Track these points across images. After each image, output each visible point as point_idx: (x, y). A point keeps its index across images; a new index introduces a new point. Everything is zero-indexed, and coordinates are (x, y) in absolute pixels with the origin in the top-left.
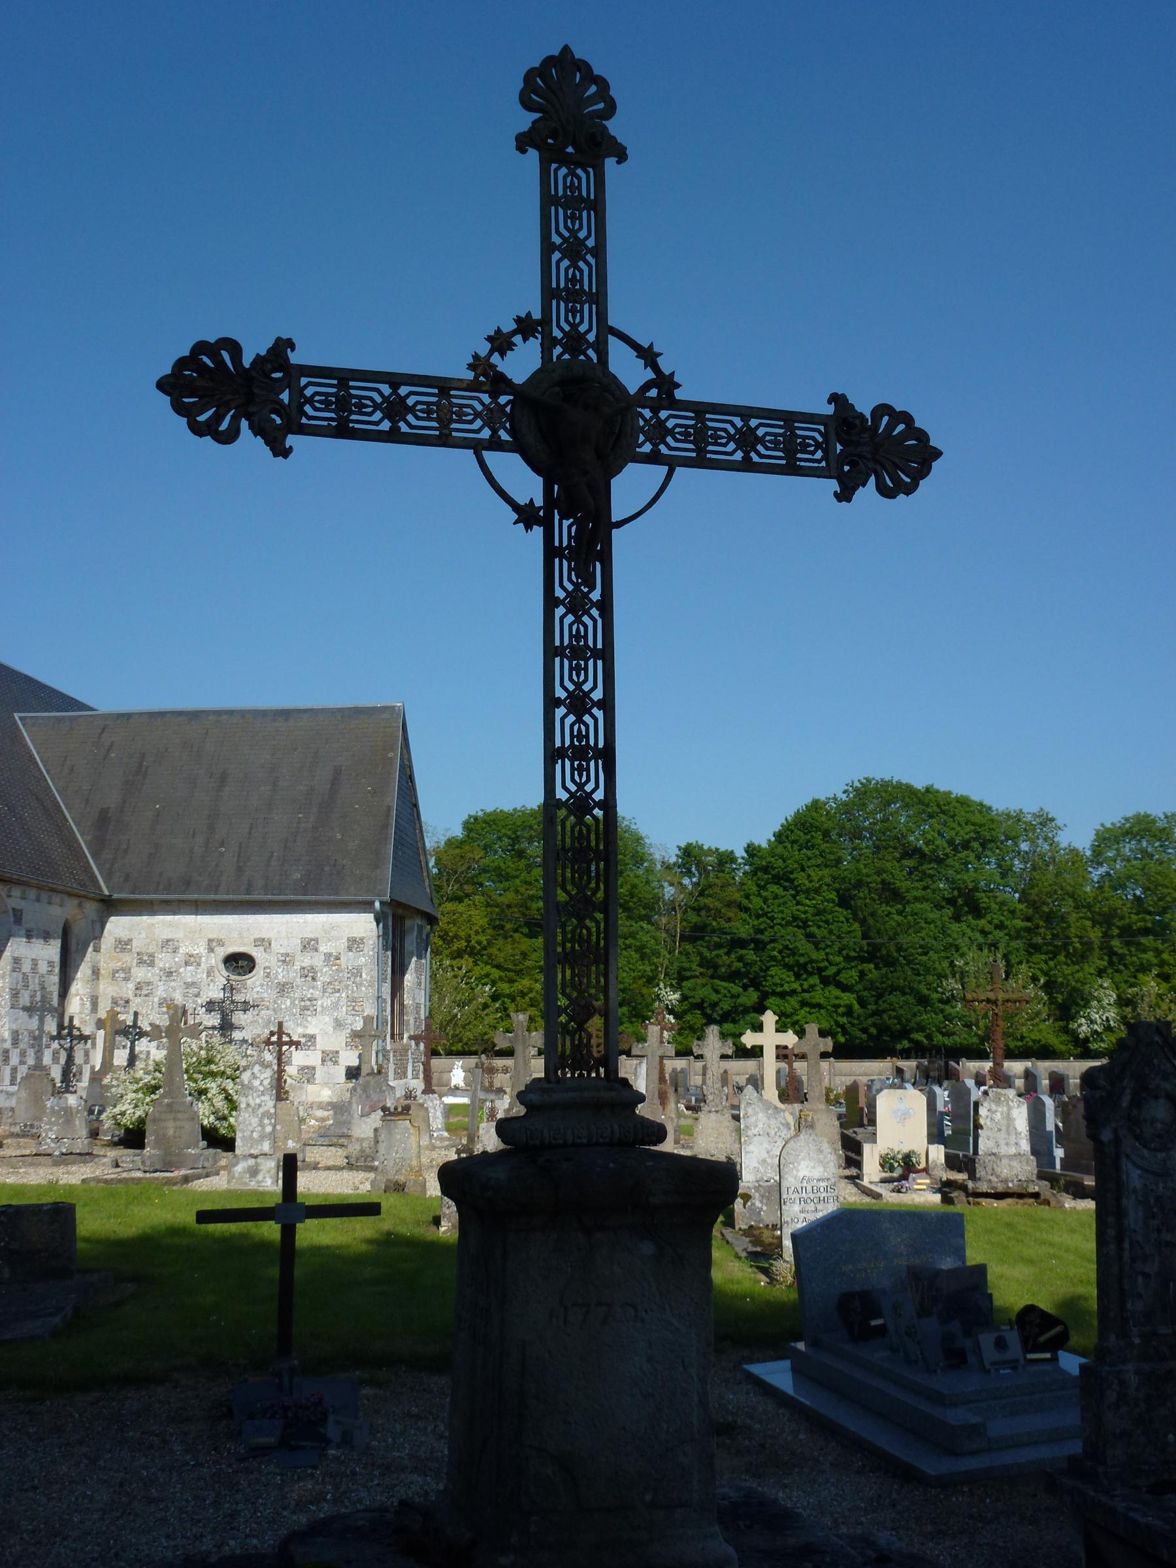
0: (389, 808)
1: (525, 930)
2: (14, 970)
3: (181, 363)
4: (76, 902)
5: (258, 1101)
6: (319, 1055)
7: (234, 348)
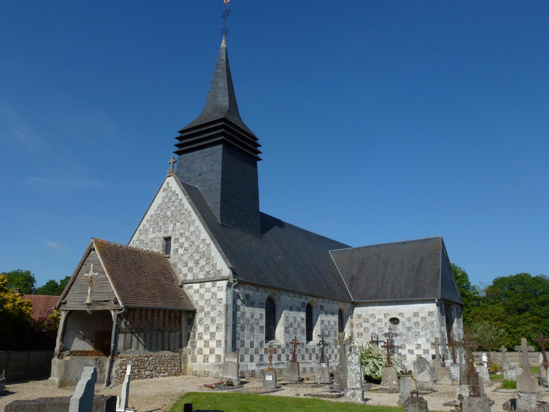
0: (439, 269)
1: (517, 312)
2: (321, 324)
4: (343, 303)
5: (354, 368)
6: (423, 351)
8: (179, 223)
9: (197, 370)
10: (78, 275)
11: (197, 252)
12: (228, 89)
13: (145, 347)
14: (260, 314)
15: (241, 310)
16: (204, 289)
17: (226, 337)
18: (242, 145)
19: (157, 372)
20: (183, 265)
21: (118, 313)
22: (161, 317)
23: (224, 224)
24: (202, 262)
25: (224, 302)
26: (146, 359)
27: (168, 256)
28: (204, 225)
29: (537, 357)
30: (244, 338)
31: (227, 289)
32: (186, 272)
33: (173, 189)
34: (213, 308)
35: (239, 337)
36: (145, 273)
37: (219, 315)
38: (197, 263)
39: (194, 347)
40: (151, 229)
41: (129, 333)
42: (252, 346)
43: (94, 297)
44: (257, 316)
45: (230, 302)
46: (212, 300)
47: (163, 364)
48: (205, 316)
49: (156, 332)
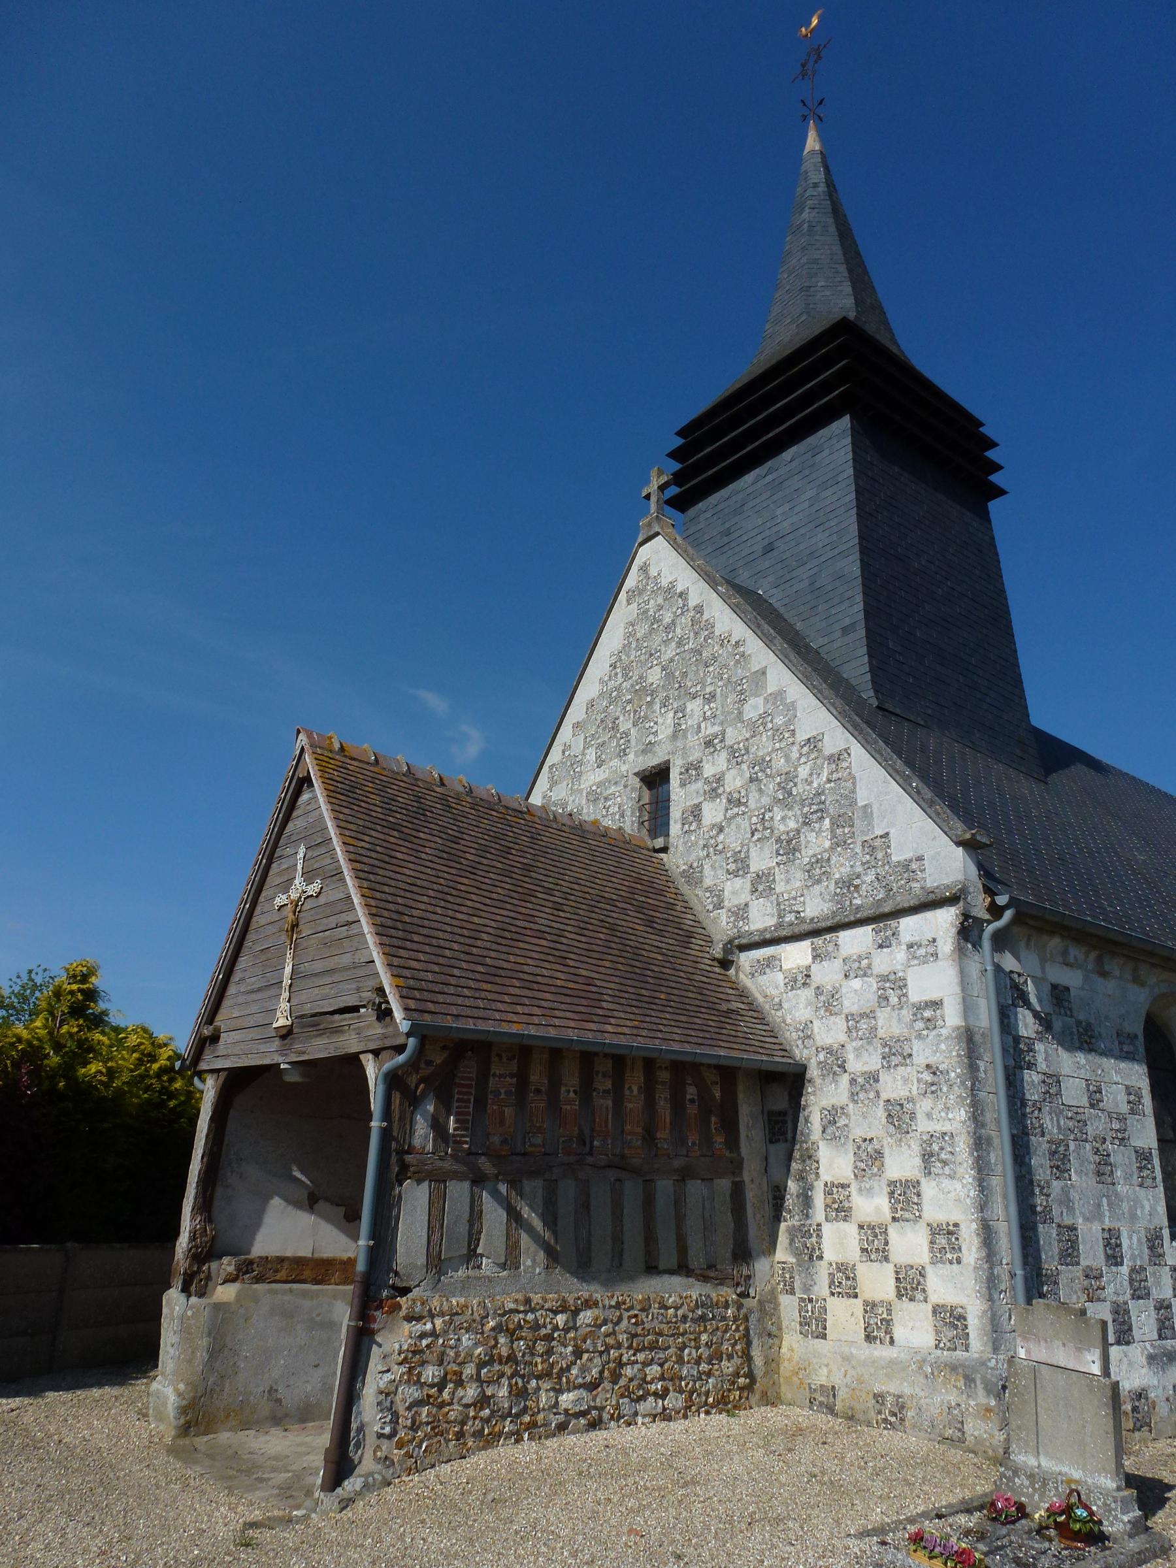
8: (699, 701)
9: (837, 1379)
10: (258, 910)
11: (786, 799)
12: (847, 262)
13: (553, 1256)
14: (1129, 1090)
15: (1042, 1066)
16: (837, 964)
17: (983, 1206)
19: (626, 1393)
20: (727, 876)
21: (387, 1066)
22: (634, 1102)
23: (887, 706)
24: (816, 842)
25: (952, 1017)
26: (561, 1319)
28: (806, 680)
30: (1071, 1210)
31: (960, 951)
32: (745, 897)
34: (896, 1053)
35: (1048, 1209)
36: (549, 892)
37: (932, 1089)
38: (789, 848)
39: (810, 1255)
40: (591, 755)
41: (457, 1176)
42: (1114, 1258)
43: (303, 996)
44: (1115, 1099)
45: (986, 1018)
46: (882, 1016)
47: (653, 1347)
48: (853, 1096)
49: (612, 1174)
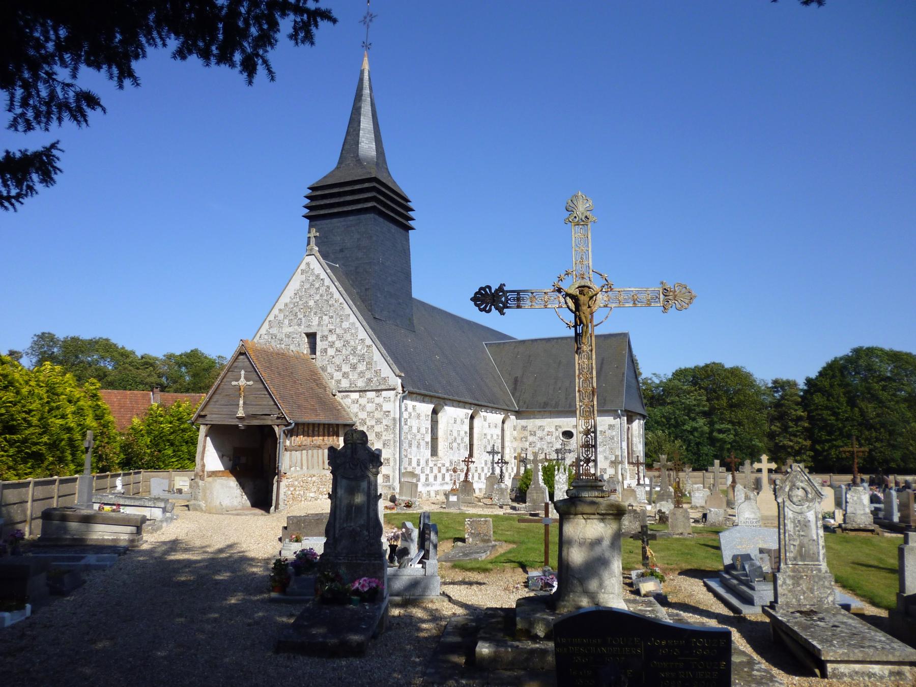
3: (476, 293)
7: (489, 287)
18: (393, 210)
24: (362, 367)
27: (314, 356)
29: (726, 478)
33: (316, 272)
37: (386, 430)
38: (354, 367)
40: (286, 322)
